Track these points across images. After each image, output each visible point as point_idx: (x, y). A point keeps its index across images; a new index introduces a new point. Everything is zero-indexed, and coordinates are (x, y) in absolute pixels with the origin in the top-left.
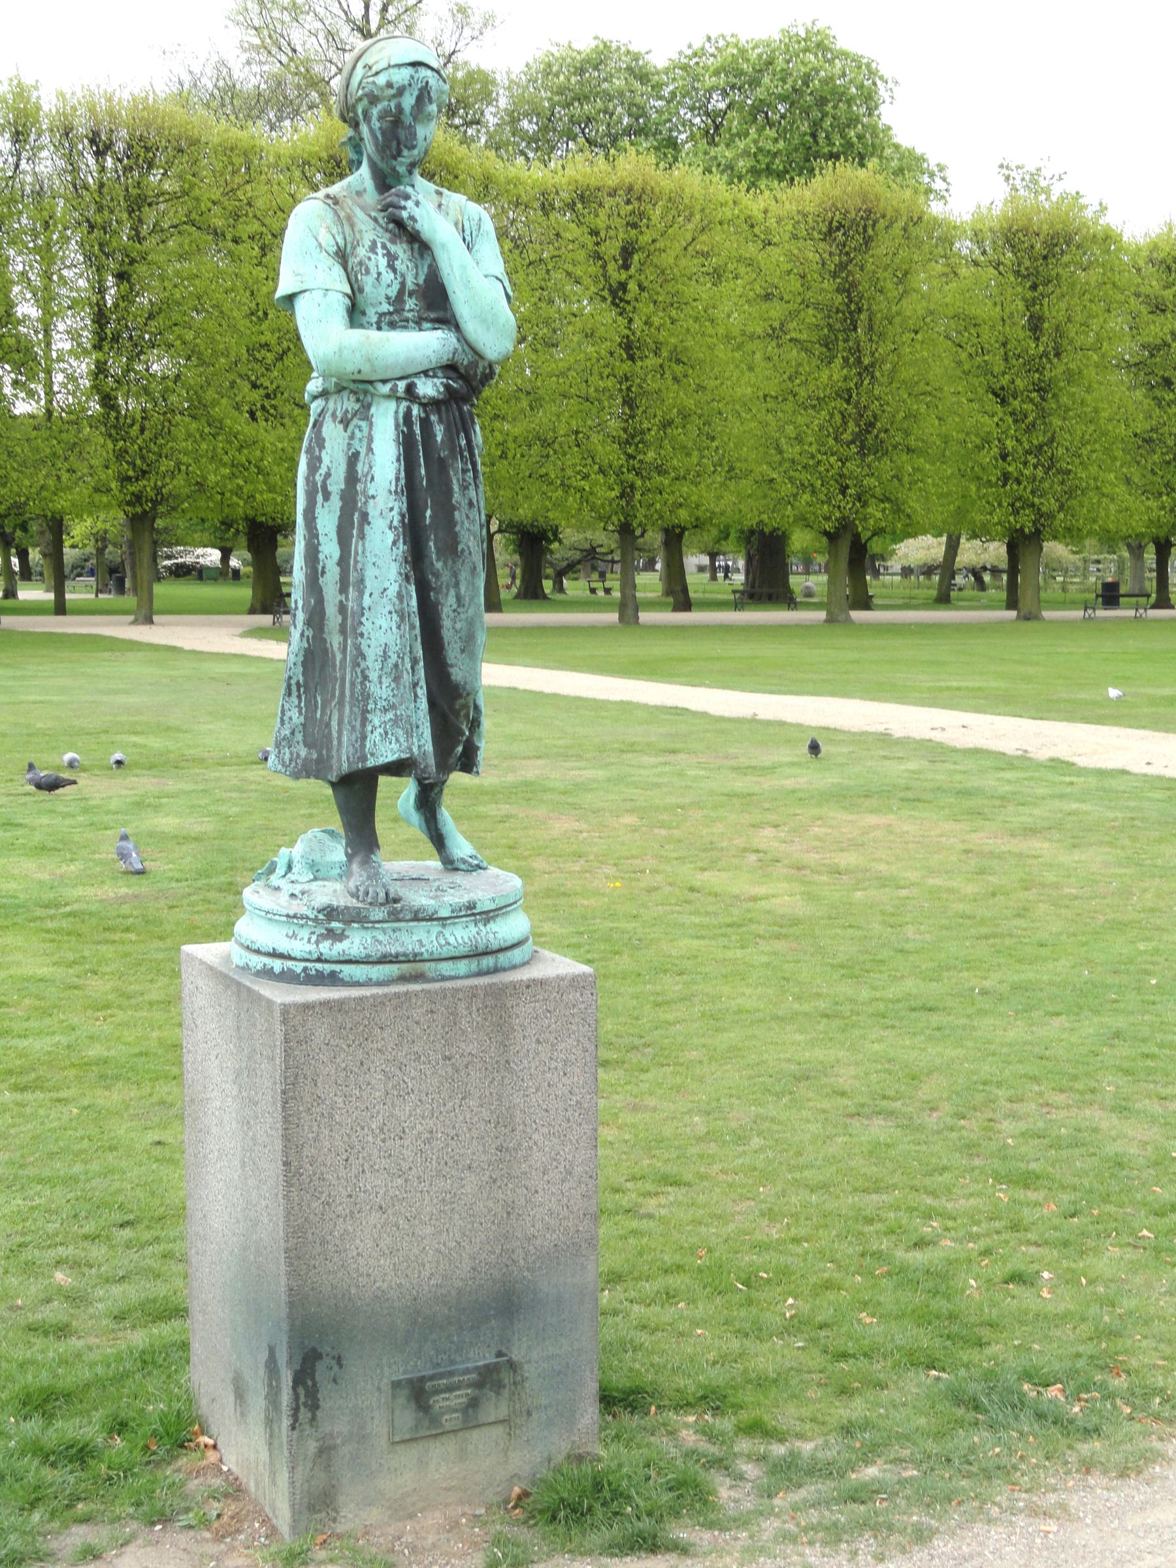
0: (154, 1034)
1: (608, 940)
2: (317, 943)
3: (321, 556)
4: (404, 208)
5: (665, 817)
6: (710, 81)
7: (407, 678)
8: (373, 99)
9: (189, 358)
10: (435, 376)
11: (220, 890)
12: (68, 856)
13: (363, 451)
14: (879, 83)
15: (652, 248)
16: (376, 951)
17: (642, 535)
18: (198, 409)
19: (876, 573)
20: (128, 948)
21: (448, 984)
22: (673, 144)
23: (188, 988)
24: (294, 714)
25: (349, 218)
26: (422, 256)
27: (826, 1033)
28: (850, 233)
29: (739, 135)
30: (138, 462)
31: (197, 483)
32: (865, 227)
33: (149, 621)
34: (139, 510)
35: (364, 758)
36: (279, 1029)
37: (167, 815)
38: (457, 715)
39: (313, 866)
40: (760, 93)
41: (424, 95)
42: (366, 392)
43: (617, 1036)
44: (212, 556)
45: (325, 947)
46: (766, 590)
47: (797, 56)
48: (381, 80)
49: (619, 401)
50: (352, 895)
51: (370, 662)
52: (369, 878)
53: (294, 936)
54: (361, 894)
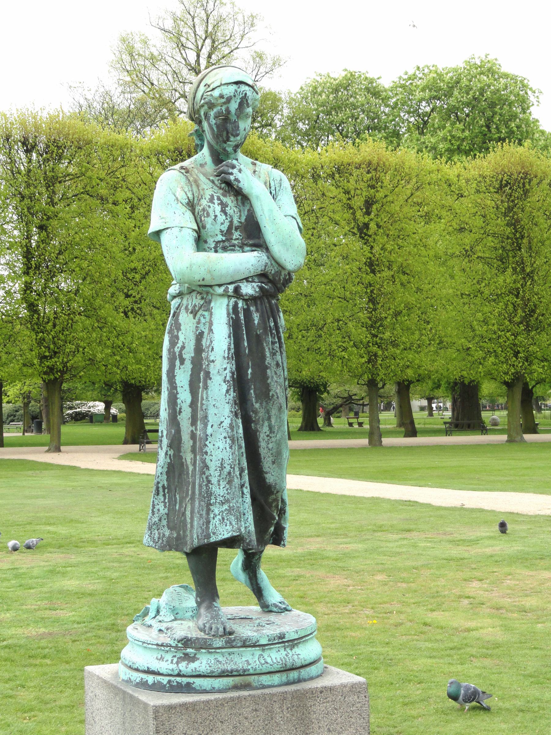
0: (63, 729)
1: (369, 660)
2: (177, 663)
3: (179, 401)
4: (232, 174)
5: (405, 575)
6: (418, 95)
7: (237, 481)
8: (211, 106)
9: (84, 279)
10: (253, 281)
11: (107, 629)
12: (5, 607)
13: (206, 331)
14: (529, 93)
15: (385, 200)
16: (218, 668)
17: (383, 387)
18: (90, 311)
19: (539, 409)
20: (44, 669)
21: (267, 691)
22: (397, 135)
23: (89, 695)
24: (161, 507)
25: (196, 181)
26: (243, 204)
27: (522, 723)
28: (513, 187)
29: (439, 128)
30: (52, 346)
31: (90, 359)
32: (524, 184)
33: (58, 450)
34: (52, 377)
35: (208, 536)
36: (152, 723)
37: (71, 579)
38: (270, 506)
39: (174, 610)
40: (452, 101)
41: (244, 102)
42: (207, 293)
43: (378, 726)
44: (99, 407)
45: (183, 666)
46: (466, 421)
47: (476, 77)
48: (216, 93)
49: (365, 300)
50: (201, 630)
51: (212, 471)
52: (212, 618)
53: (162, 659)
54: (207, 629)
